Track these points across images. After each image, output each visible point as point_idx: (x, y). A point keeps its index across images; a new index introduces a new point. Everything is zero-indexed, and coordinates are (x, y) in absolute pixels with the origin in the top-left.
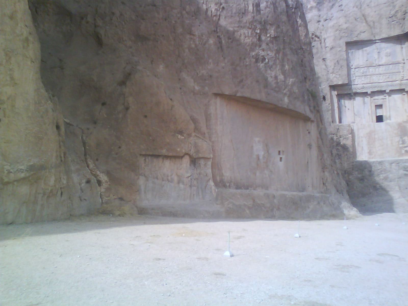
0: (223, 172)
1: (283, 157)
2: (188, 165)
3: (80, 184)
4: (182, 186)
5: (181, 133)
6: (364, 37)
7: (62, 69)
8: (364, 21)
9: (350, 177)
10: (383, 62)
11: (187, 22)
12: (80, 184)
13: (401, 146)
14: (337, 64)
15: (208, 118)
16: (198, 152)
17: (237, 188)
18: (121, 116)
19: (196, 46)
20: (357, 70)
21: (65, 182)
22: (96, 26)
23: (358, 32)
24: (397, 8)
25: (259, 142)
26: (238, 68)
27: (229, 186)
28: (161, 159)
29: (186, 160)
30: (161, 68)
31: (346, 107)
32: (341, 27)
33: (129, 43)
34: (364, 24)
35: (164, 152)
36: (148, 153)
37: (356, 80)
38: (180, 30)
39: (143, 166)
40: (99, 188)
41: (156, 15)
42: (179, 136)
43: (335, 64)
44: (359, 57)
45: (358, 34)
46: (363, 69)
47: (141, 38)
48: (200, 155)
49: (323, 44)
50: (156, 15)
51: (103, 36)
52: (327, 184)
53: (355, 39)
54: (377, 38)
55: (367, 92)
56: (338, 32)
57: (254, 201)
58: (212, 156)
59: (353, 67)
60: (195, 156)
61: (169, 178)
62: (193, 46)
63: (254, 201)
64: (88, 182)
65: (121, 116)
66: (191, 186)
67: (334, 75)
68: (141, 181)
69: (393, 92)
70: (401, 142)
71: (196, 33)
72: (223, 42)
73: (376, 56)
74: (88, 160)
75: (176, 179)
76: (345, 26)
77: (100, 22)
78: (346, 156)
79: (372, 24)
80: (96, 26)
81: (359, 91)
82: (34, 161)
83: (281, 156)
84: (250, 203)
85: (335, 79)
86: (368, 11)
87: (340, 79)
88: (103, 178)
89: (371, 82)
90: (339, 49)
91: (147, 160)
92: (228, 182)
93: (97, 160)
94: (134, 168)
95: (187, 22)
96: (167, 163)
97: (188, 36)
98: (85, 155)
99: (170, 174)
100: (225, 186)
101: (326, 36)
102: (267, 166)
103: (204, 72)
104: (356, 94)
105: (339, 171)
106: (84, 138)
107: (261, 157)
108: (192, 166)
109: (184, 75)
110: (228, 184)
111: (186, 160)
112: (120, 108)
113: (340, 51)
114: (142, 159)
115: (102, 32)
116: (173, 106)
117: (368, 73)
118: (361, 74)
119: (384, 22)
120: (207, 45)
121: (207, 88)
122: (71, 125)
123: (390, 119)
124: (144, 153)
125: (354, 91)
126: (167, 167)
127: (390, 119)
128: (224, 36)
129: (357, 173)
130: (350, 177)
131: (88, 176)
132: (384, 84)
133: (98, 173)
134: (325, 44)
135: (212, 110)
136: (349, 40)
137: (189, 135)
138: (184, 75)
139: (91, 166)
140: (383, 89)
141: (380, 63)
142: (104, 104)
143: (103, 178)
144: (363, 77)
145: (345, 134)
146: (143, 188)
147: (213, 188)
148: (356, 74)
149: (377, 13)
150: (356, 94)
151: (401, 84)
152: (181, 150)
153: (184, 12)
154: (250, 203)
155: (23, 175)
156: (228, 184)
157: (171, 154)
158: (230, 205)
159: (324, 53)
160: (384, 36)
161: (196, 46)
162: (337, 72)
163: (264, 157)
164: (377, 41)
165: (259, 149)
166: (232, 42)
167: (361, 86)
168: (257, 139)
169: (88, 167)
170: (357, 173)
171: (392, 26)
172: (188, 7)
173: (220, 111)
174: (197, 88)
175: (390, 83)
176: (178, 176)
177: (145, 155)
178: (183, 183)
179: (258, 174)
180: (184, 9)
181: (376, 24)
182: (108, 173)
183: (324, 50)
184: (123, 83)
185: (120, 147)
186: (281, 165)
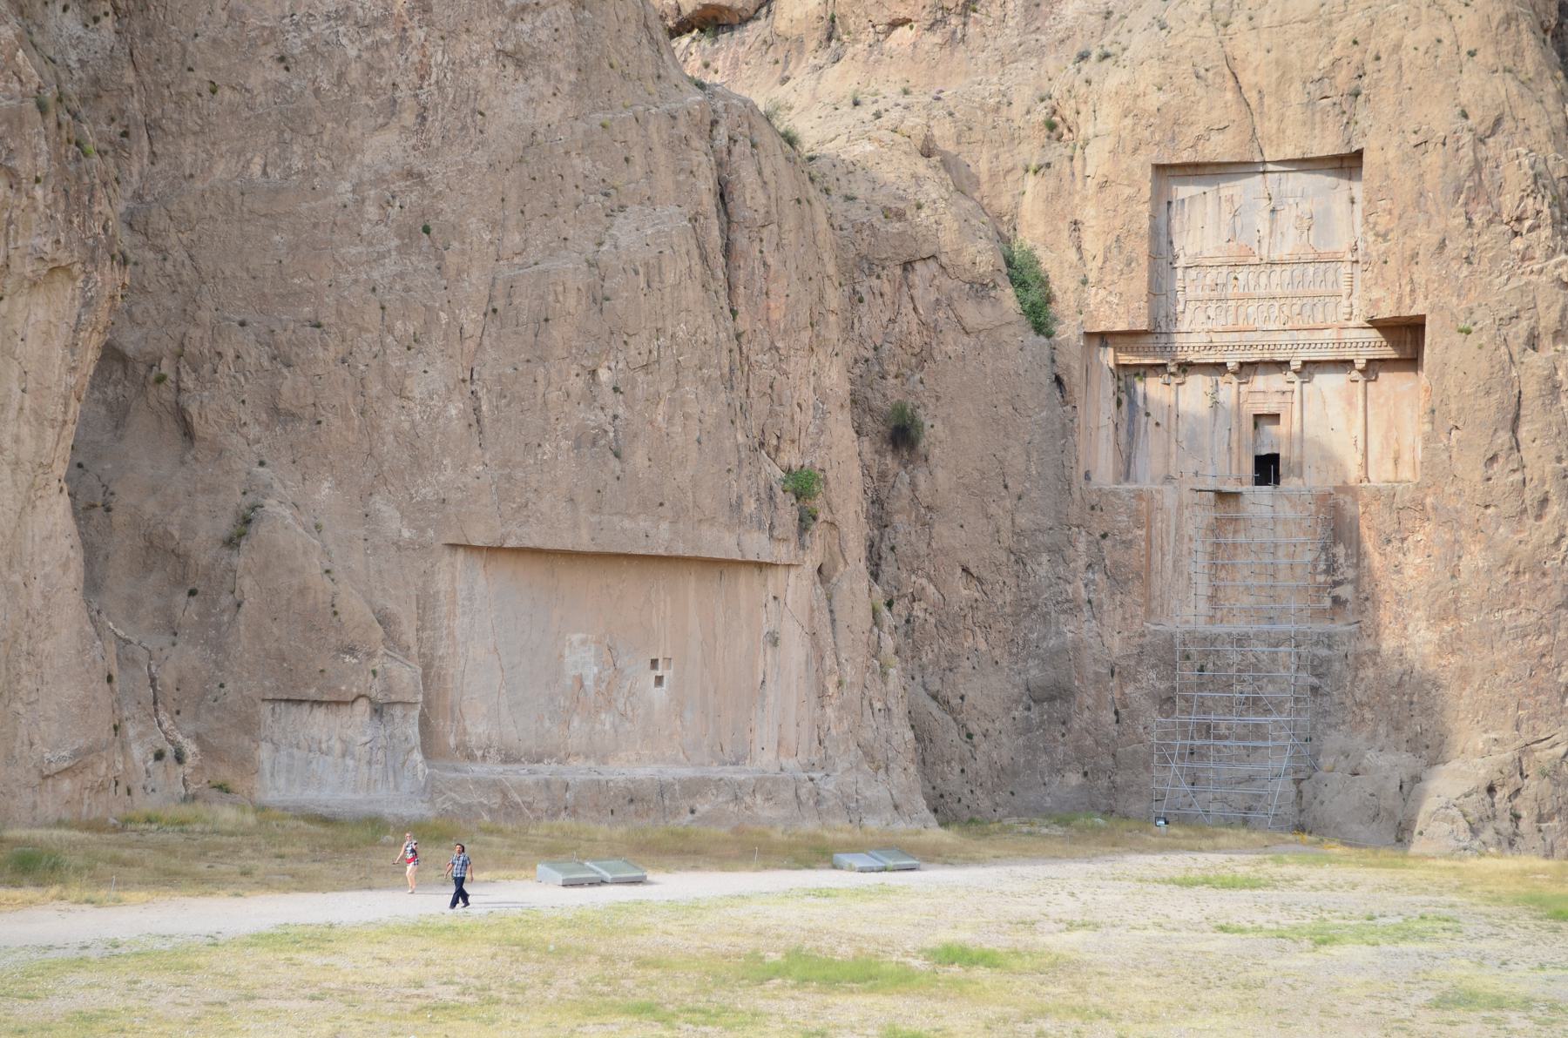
0: (468, 723)
1: (668, 675)
2: (367, 718)
3: (145, 762)
4: (350, 762)
5: (351, 650)
6: (1219, 148)
7: (108, 510)
8: (1231, 83)
9: (1129, 689)
10: (1284, 250)
11: (395, 364)
12: (145, 762)
13: (1321, 578)
14: (1115, 251)
15: (426, 604)
16: (388, 689)
17: (505, 761)
18: (226, 618)
19: (414, 425)
20: (1193, 273)
21: (121, 767)
22: (179, 390)
23: (1199, 129)
24: (1337, 51)
25: (583, 642)
26: (519, 474)
27: (484, 756)
28: (306, 707)
29: (362, 707)
30: (325, 490)
31: (1148, 414)
32: (1140, 102)
33: (254, 431)
34: (1229, 96)
35: (312, 693)
36: (278, 696)
37: (1188, 315)
38: (375, 388)
39: (269, 721)
40: (180, 769)
41: (321, 354)
42: (348, 659)
43: (1108, 250)
44: (1203, 222)
45: (1199, 138)
46: (1214, 272)
47: (278, 414)
48: (393, 698)
49: (1078, 163)
50: (321, 354)
51: (196, 419)
52: (827, 743)
53: (1186, 157)
54: (1269, 155)
55: (1224, 364)
56: (1129, 121)
57: (505, 795)
58: (420, 698)
59: (1181, 262)
60: (381, 698)
61: (324, 746)
62: (406, 426)
63: (505, 795)
64: (159, 756)
65: (226, 618)
66: (369, 763)
67: (1102, 293)
68: (264, 753)
69: (1311, 367)
70: (1322, 566)
71: (417, 394)
72: (484, 408)
73: (1261, 222)
74: (161, 713)
75: (338, 747)
76: (1154, 100)
77: (189, 381)
78: (1120, 611)
79: (1252, 96)
80: (179, 390)
81: (1193, 357)
82: (81, 742)
83: (659, 673)
84: (496, 801)
85: (1104, 309)
86: (1245, 44)
87: (1121, 310)
88: (190, 748)
89: (1241, 326)
90: (1128, 191)
91: (278, 710)
92: (479, 748)
93: (178, 713)
94: (248, 726)
95: (395, 364)
96: (320, 714)
97: (396, 401)
98: (155, 703)
99: (324, 738)
100: (470, 757)
101: (1091, 131)
102: (610, 702)
103: (428, 492)
104: (1186, 367)
105: (892, 702)
106: (153, 669)
107: (588, 683)
108: (376, 719)
109: (379, 503)
110: (479, 753)
111: (362, 707)
112: (226, 600)
113: (1130, 198)
114: (266, 709)
115: (193, 409)
116: (334, 595)
117: (1230, 292)
118: (1207, 293)
119: (1295, 95)
120: (441, 421)
121: (431, 533)
122: (129, 642)
123: (1301, 476)
124: (270, 696)
125: (1181, 357)
126: (318, 723)
127: (1301, 476)
128: (489, 391)
129: (1153, 675)
130: (1129, 689)
131: (159, 746)
132: (1285, 337)
133: (180, 738)
134: (1084, 167)
135: (442, 583)
136: (1159, 162)
137: (370, 655)
138: (379, 503)
139: (166, 725)
140: (1279, 357)
141: (1275, 256)
142: (192, 593)
143: (190, 748)
144: (1213, 305)
145: (1122, 525)
146: (267, 766)
147: (420, 766)
148: (1190, 293)
149: (1273, 55)
150: (1186, 367)
151: (1340, 344)
152: (346, 689)
153: (389, 339)
154: (496, 801)
155: (66, 765)
156: (479, 753)
157: (326, 698)
158: (448, 806)
159: (1077, 199)
160: (1290, 152)
161: (414, 425)
162: (1113, 283)
163: (598, 680)
164: (1270, 167)
165: (581, 659)
166: (509, 405)
167: (1205, 339)
168: (576, 638)
169: (160, 725)
170: (1153, 675)
171: (1318, 117)
172: (399, 324)
173: (461, 581)
174: (406, 534)
175: (1303, 335)
176: (343, 741)
177: (273, 700)
178: (353, 757)
179: (576, 723)
180: (390, 330)
181: (1267, 101)
182: (198, 738)
183: (1079, 186)
184: (232, 543)
185: (222, 686)
186: (660, 695)
